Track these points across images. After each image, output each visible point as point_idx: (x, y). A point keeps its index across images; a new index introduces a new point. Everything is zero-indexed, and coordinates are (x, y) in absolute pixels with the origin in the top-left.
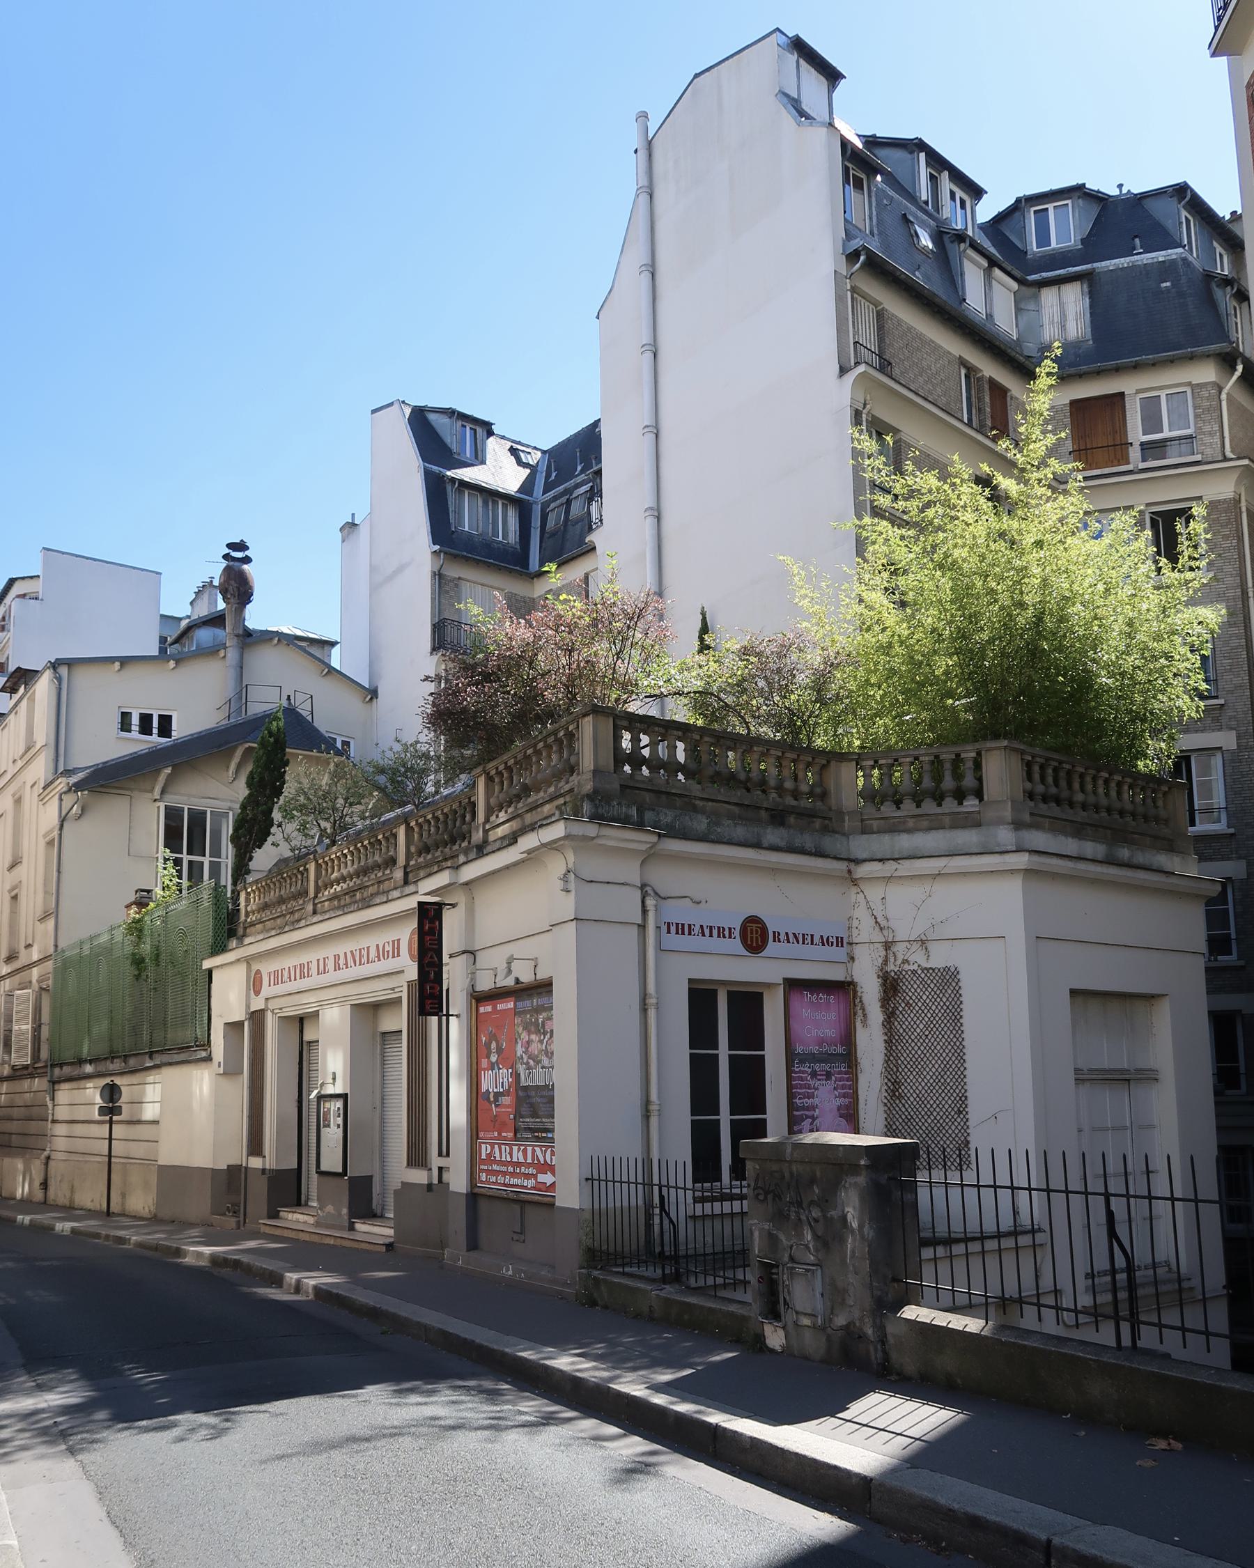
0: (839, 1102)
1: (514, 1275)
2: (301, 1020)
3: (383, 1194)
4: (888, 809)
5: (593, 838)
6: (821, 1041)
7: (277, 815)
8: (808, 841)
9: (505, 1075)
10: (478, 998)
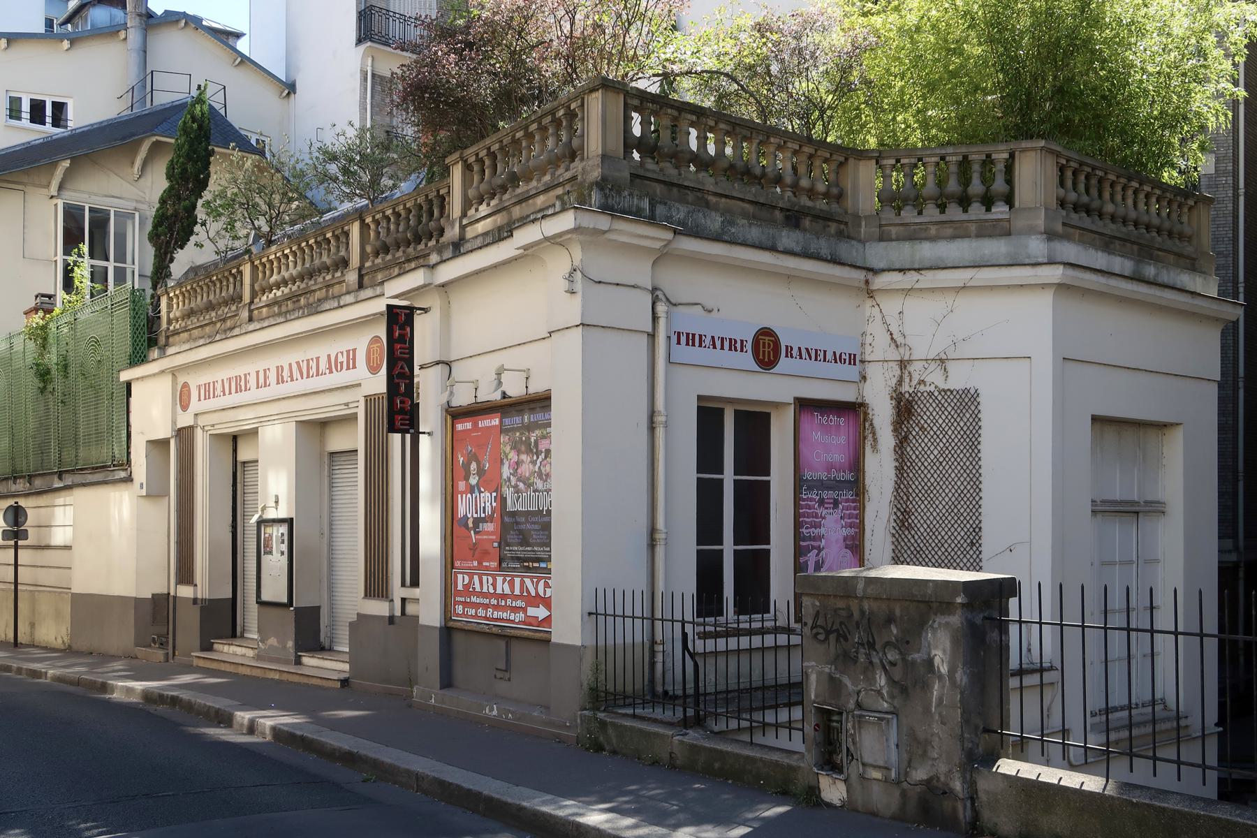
0: (845, 532)
1: (499, 715)
2: (235, 438)
3: (332, 626)
4: (909, 215)
5: (605, 232)
6: (830, 467)
7: (200, 213)
8: (823, 246)
9: (487, 500)
10: (455, 414)
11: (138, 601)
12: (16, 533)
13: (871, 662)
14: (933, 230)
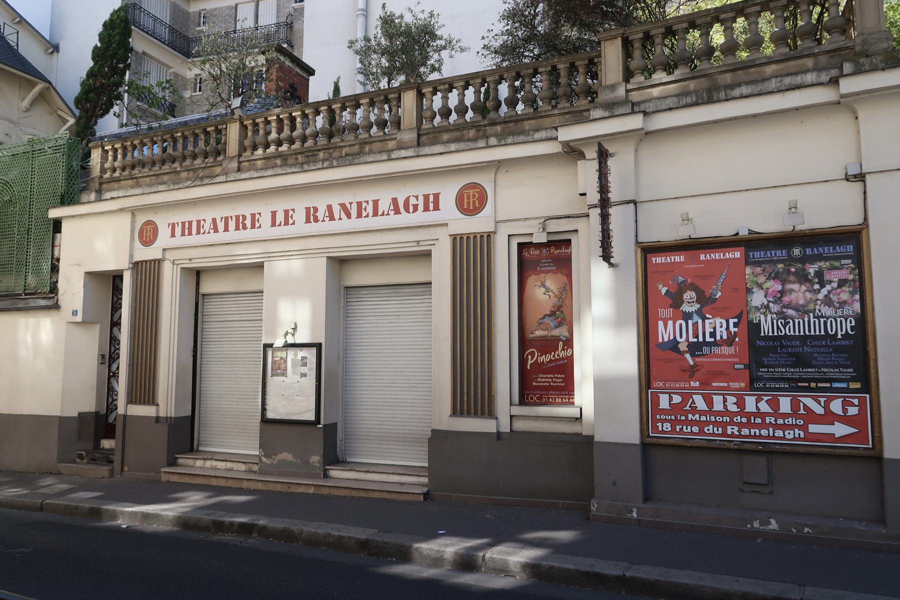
10: (648, 250)
11: (63, 421)
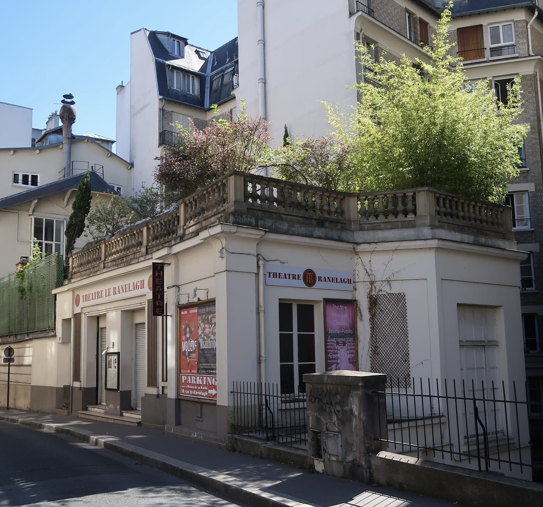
0: (349, 356)
2: (98, 318)
3: (136, 399)
4: (372, 219)
5: (234, 233)
6: (341, 328)
7: (86, 222)
8: (335, 234)
10: (181, 307)
12: (9, 359)
13: (331, 411)
14: (383, 226)
